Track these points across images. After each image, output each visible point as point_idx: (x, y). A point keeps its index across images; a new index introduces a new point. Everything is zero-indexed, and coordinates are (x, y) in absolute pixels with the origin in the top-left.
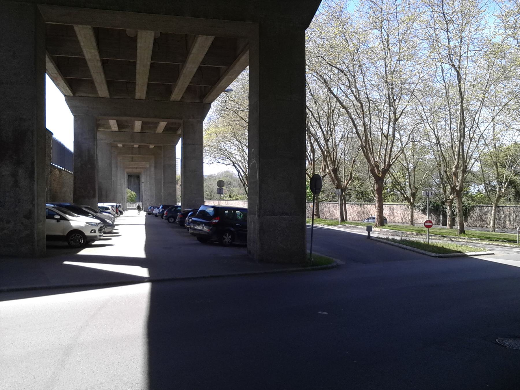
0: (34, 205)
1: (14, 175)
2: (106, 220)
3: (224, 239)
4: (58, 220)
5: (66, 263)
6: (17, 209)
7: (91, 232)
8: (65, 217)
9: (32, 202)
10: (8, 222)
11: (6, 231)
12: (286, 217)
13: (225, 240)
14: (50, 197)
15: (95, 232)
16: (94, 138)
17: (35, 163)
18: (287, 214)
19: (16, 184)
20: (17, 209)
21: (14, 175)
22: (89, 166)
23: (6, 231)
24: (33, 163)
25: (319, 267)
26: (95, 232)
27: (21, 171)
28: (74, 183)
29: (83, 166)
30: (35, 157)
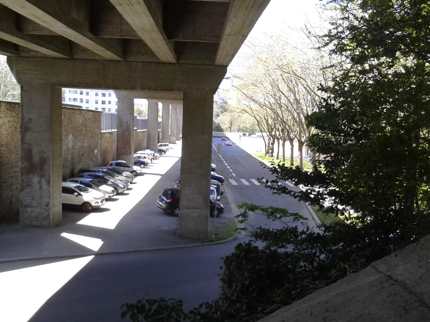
0: (50, 199)
1: (40, 182)
2: (119, 185)
3: (175, 212)
4: (77, 196)
5: (64, 235)
6: (41, 201)
7: (95, 203)
8: (80, 193)
9: (49, 198)
10: (37, 208)
11: (35, 213)
12: (197, 210)
13: (175, 213)
14: (100, 154)
15: (98, 203)
16: (131, 114)
17: (51, 176)
18: (197, 209)
19: (41, 188)
20: (41, 201)
21: (40, 182)
22: (127, 133)
23: (35, 213)
24: (50, 176)
25: (224, 241)
26: (98, 203)
27: (43, 181)
28: (117, 145)
29: (123, 133)
30: (51, 173)
